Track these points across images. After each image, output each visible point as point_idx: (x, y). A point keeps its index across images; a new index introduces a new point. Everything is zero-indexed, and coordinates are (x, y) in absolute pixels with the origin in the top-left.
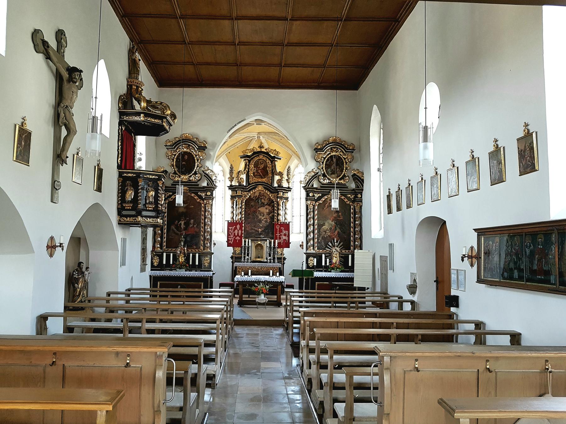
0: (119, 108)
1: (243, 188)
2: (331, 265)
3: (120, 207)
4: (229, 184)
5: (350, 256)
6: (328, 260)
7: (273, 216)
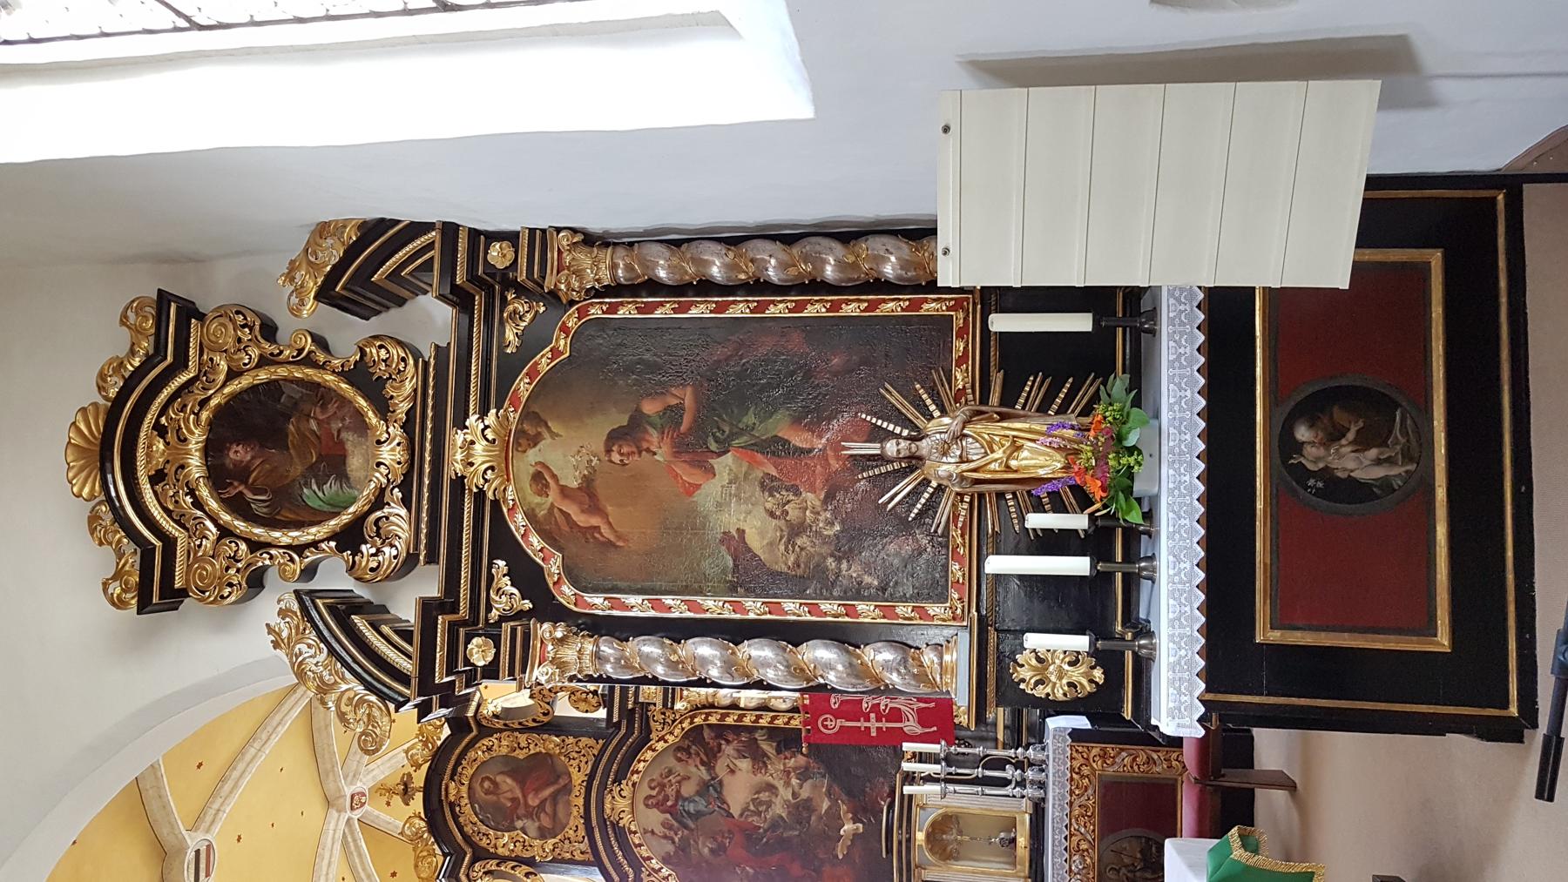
2: (1084, 501)
5: (1002, 323)
6: (1036, 521)
7: (772, 732)
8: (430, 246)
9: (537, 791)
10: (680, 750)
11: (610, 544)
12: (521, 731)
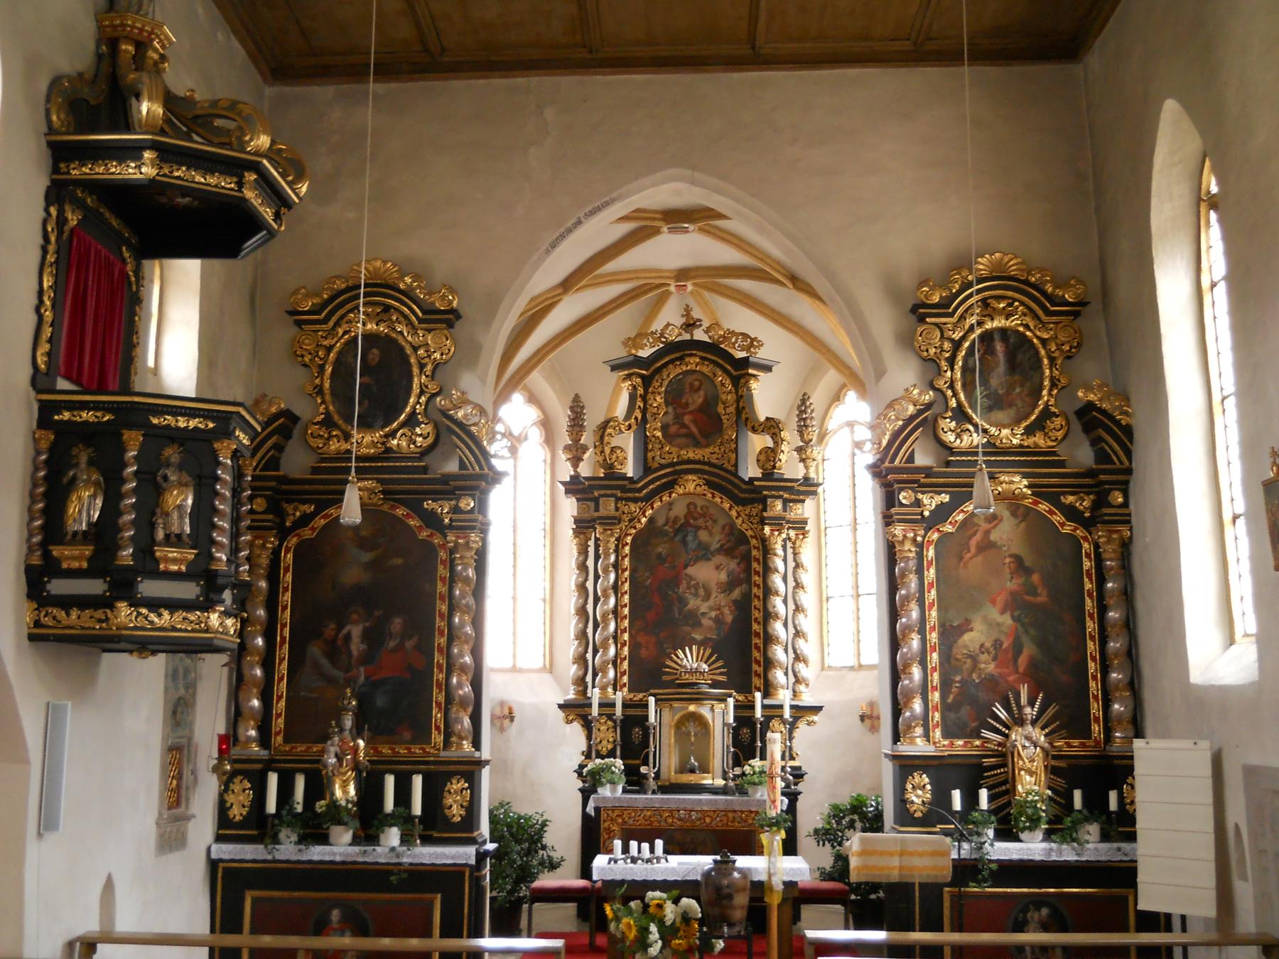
0: (51, 130)
1: (623, 489)
3: (36, 560)
4: (566, 472)
8: (1121, 463)
9: (695, 422)
10: (731, 528)
11: (961, 558)
12: (737, 408)
